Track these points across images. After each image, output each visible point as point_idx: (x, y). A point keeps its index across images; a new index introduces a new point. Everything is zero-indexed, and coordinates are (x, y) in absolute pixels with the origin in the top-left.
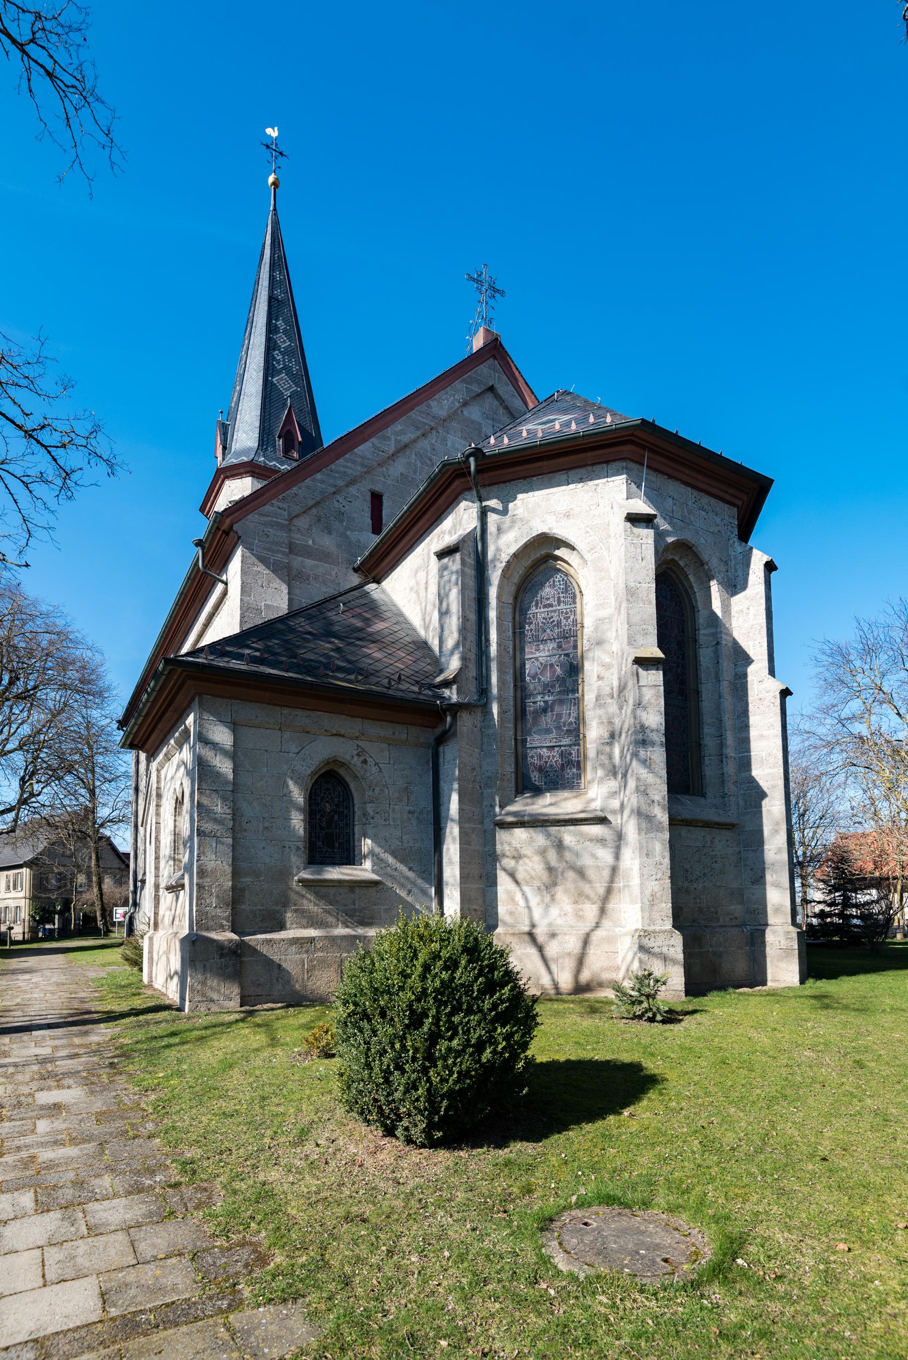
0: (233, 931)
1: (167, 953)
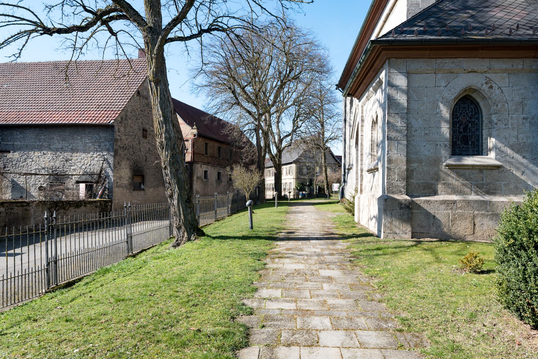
0: (407, 195)
1: (369, 205)
